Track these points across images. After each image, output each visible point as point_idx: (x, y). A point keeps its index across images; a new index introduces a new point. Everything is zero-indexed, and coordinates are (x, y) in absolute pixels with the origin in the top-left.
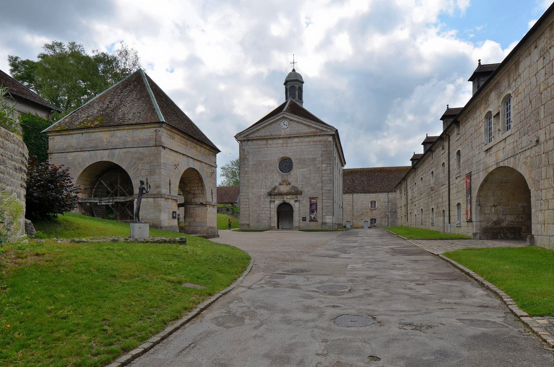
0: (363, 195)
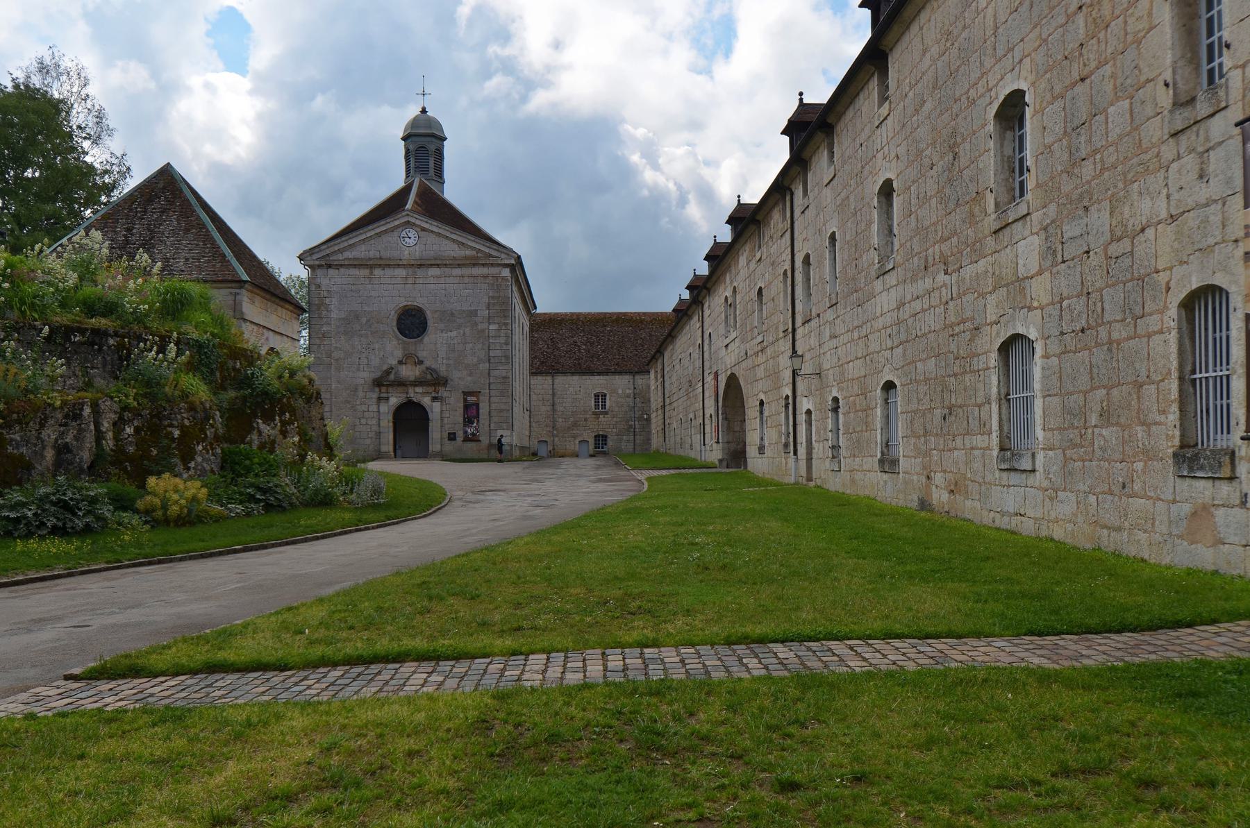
0: (576, 378)
